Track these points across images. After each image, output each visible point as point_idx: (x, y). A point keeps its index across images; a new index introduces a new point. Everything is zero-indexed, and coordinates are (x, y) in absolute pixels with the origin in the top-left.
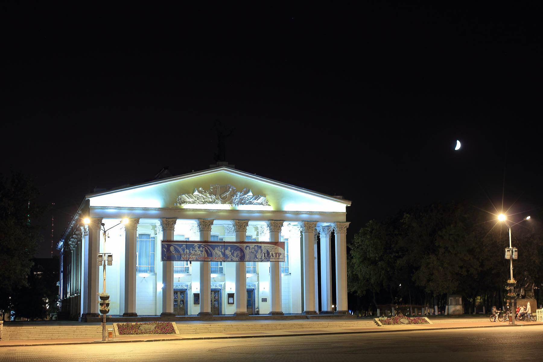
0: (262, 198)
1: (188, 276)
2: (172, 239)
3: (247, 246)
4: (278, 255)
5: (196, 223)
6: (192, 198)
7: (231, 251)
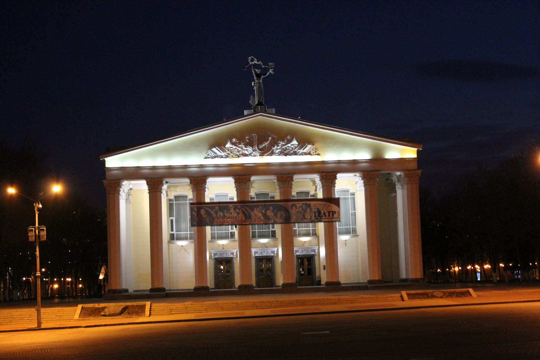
0: (309, 146)
1: (224, 243)
2: (202, 201)
3: (293, 205)
4: (331, 214)
5: (318, 177)
6: (224, 151)
7: (273, 212)
